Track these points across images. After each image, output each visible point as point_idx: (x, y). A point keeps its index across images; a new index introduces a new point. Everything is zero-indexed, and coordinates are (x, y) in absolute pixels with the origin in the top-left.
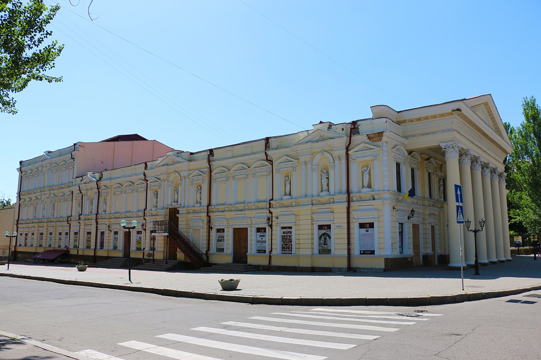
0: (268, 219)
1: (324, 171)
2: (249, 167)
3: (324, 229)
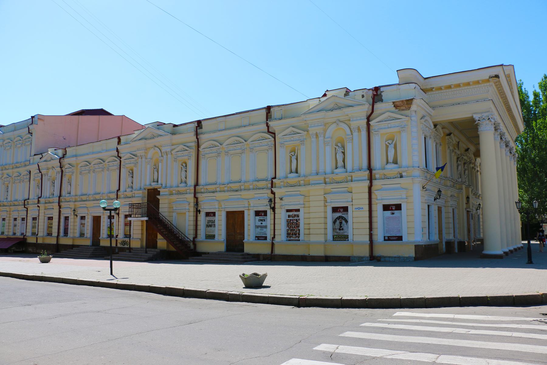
0: (270, 200)
1: (339, 145)
2: (246, 141)
3: (340, 211)
